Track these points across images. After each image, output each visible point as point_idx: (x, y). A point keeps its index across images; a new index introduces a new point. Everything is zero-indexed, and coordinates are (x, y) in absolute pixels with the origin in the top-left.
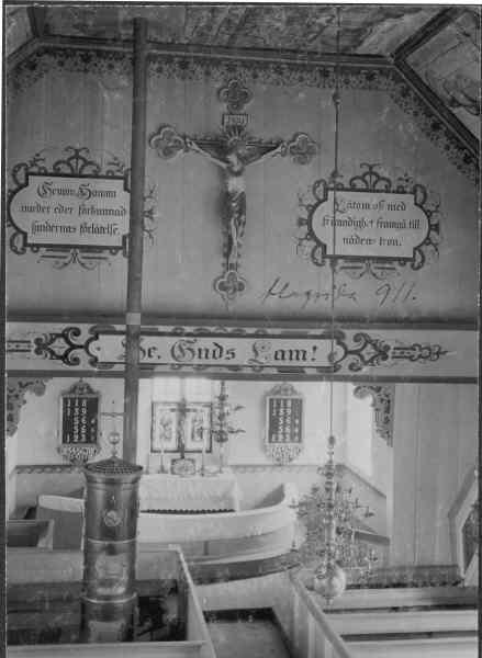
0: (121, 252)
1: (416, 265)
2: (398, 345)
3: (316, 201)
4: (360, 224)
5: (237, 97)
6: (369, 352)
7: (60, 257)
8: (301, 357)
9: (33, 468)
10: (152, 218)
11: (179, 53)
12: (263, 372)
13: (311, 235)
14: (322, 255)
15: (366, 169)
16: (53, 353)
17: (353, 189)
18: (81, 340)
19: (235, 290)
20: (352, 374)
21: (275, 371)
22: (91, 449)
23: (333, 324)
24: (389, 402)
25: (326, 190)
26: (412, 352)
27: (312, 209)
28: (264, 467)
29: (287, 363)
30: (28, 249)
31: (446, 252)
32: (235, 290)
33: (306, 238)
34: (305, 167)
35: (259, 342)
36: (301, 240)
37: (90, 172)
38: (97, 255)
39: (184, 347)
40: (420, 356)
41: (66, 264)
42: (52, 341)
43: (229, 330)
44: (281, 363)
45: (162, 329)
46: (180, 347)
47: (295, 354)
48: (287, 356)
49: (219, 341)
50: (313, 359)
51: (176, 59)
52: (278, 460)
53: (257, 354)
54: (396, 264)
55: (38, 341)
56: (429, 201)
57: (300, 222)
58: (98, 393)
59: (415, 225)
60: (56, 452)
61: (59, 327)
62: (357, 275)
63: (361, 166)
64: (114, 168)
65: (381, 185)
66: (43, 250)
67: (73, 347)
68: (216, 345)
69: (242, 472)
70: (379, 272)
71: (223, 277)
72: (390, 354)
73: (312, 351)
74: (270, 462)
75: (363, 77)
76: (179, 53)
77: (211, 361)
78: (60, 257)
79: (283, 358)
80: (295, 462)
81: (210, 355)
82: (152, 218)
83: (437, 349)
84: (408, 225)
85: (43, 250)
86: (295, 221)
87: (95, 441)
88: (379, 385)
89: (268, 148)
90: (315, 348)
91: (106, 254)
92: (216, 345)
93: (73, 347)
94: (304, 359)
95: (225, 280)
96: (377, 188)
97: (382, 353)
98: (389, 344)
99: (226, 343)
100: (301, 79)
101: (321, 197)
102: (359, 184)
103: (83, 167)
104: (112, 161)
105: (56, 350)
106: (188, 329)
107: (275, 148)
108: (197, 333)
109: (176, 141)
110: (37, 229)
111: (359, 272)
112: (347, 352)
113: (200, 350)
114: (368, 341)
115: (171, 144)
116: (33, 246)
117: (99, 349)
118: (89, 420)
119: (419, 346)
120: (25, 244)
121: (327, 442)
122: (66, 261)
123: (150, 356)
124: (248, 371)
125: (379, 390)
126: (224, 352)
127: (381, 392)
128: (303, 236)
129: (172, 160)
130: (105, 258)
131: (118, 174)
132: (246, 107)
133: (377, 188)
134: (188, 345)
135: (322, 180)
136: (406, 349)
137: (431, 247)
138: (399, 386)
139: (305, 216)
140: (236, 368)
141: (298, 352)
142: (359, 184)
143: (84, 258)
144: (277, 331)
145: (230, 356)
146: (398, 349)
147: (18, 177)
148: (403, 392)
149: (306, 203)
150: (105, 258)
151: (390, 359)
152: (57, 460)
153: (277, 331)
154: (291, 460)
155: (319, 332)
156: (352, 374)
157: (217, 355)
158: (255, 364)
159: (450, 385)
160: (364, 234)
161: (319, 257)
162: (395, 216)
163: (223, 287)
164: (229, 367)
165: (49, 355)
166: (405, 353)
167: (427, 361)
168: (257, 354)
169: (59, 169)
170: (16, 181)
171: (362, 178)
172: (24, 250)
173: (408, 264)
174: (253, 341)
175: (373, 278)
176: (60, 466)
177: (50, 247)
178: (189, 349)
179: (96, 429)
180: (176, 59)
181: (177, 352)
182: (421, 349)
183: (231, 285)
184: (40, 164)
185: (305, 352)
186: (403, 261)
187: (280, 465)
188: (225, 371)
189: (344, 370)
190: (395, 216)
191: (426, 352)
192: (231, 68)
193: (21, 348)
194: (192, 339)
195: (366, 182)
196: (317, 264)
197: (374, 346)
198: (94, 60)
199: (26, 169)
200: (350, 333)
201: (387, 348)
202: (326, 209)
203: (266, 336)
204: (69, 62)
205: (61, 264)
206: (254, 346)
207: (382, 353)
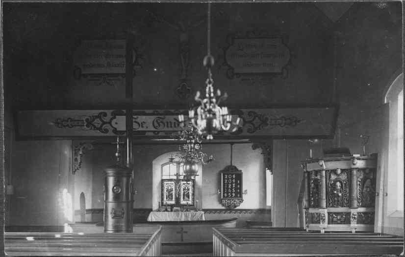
30: (235, 76)
42: (94, 120)
46: (157, 121)
55: (87, 120)
61: (96, 112)
83: (60, 126)
105: (96, 125)
114: (100, 129)
117: (116, 123)
138: (275, 141)
151: (269, 126)
165: (93, 128)
178: (162, 122)
181: (156, 124)
193: (80, 124)
194: (162, 117)
197: (260, 118)
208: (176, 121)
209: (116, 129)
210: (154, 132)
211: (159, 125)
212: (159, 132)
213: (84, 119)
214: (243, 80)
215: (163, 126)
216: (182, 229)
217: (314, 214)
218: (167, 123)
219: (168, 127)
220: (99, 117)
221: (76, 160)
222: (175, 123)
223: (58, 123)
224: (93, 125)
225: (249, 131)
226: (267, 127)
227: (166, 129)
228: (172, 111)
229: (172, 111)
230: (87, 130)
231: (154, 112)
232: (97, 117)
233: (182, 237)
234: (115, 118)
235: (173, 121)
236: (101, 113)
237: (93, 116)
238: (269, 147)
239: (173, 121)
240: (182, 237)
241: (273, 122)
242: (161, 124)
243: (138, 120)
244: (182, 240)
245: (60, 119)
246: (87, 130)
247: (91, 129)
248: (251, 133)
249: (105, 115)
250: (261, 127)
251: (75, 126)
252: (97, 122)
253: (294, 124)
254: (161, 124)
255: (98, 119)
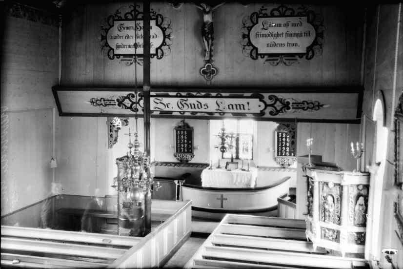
0: (156, 57)
1: (309, 57)
2: (294, 101)
4: (278, 35)
6: (278, 105)
7: (130, 60)
8: (242, 108)
9: (162, 164)
10: (169, 39)
12: (197, 115)
14: (255, 54)
16: (126, 106)
18: (269, 109)
19: (211, 74)
20: (272, 117)
22: (189, 156)
23: (256, 90)
24: (294, 132)
26: (303, 106)
28: (275, 168)
30: (115, 57)
31: (326, 49)
33: (247, 45)
35: (219, 100)
36: (245, 46)
37: (289, 14)
39: (183, 103)
40: (308, 108)
42: (124, 100)
45: (171, 94)
46: (181, 103)
47: (238, 106)
48: (235, 107)
49: (200, 100)
50: (249, 109)
52: (283, 165)
54: (297, 57)
55: (118, 100)
57: (244, 36)
58: (192, 128)
59: (308, 34)
60: (173, 156)
61: (125, 94)
65: (288, 13)
68: (198, 101)
69: (264, 170)
70: (287, 62)
71: (204, 67)
72: (290, 106)
73: (247, 105)
74: (279, 166)
77: (197, 110)
78: (130, 60)
79: (233, 108)
80: (291, 166)
83: (317, 104)
84: (303, 35)
85: (122, 57)
87: (192, 152)
88: (288, 123)
90: (248, 103)
92: (198, 101)
94: (244, 109)
95: (205, 68)
96: (286, 14)
97: (286, 106)
98: (289, 101)
99: (203, 101)
102: (130, 17)
103: (286, 11)
105: (126, 104)
106: (184, 94)
108: (188, 96)
110: (118, 47)
118: (188, 141)
119: (307, 102)
121: (118, 140)
123: (168, 107)
125: (288, 126)
126: (203, 106)
127: (290, 127)
131: (304, 14)
133: (286, 14)
134: (184, 102)
135: (256, 13)
136: (299, 103)
137: (166, 47)
138: (299, 124)
141: (240, 105)
143: (139, 60)
144: (227, 94)
145: (206, 107)
146: (295, 103)
148: (301, 128)
150: (296, 60)
151: (291, 109)
152: (174, 160)
154: (289, 165)
156: (272, 117)
157: (200, 107)
159: (309, 124)
160: (278, 41)
161: (254, 55)
162: (297, 30)
163: (204, 72)
165: (124, 107)
166: (299, 106)
167: (313, 110)
170: (109, 25)
171: (130, 13)
172: (257, 58)
173: (305, 57)
174: (215, 99)
175: (284, 65)
176: (173, 163)
177: (125, 56)
178: (185, 104)
179: (192, 146)
182: (308, 104)
183: (208, 71)
184: (119, 15)
185: (243, 105)
186: (301, 55)
187: (284, 168)
188: (206, 115)
189: (267, 115)
190: (297, 30)
191: (311, 105)
193: (112, 103)
194: (185, 99)
196: (253, 58)
197: (281, 102)
199: (113, 18)
200: (266, 96)
201: (288, 103)
202: (257, 28)
203: (222, 97)
205: (130, 64)
206: (217, 102)
207: (286, 106)
209: (260, 100)
210: (180, 112)
212: (184, 112)
213: (116, 100)
215: (218, 102)
216: (222, 196)
217: (289, 156)
218: (191, 104)
219: (191, 108)
220: (128, 97)
221: (111, 136)
222: (198, 105)
223: (93, 102)
224: (125, 105)
226: (289, 111)
227: (190, 110)
228: (195, 94)
229: (195, 94)
230: (289, 98)
231: (177, 94)
232: (126, 98)
233: (222, 204)
234: (261, 111)
235: (196, 103)
236: (129, 95)
238: (293, 129)
240: (222, 204)
241: (295, 106)
242: (185, 105)
243: (188, 103)
244: (222, 207)
245: (94, 99)
246: (289, 98)
247: (285, 99)
248: (131, 94)
249: (271, 113)
251: (108, 105)
252: (127, 102)
253: (317, 108)
255: (128, 100)
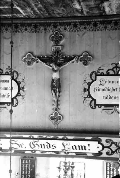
3: (91, 81)
5: (57, 39)
10: (23, 91)
11: (113, 19)
13: (89, 96)
15: (114, 65)
17: (108, 75)
21: (74, 154)
25: (96, 75)
27: (89, 84)
29: (78, 151)
30: (97, 106)
32: (57, 119)
33: (87, 97)
34: (86, 67)
35: (65, 142)
38: (2, 106)
41: (112, 113)
43: (52, 137)
44: (75, 151)
48: (78, 148)
49: (49, 141)
51: (53, 24)
53: (65, 147)
56: (19, 77)
57: (85, 90)
62: (110, 113)
63: (112, 64)
64: (8, 71)
66: (103, 107)
67: (108, 147)
75: (92, 25)
76: (113, 19)
77: (46, 149)
81: (46, 147)
82: (23, 91)
86: (82, 90)
89: (70, 59)
90: (89, 145)
91: (6, 105)
93: (108, 147)
99: (52, 142)
100: (85, 28)
101: (94, 79)
104: (8, 68)
107: (73, 59)
108: (39, 138)
109: (33, 58)
111: (111, 111)
112: (104, 147)
113: (41, 145)
114: (113, 143)
115: (30, 60)
116: (98, 105)
117: (98, 148)
120: (95, 104)
122: (113, 111)
124: (63, 154)
128: (86, 96)
129: (31, 67)
130: (5, 107)
132: (62, 42)
137: (21, 97)
139: (87, 87)
140: (58, 152)
141: (82, 146)
142: (111, 72)
144: (72, 138)
147: (92, 77)
149: (87, 82)
150: (5, 107)
153: (72, 138)
155: (90, 138)
158: (65, 151)
161: (93, 105)
163: (52, 118)
164: (55, 152)
168: (65, 147)
169: (109, 73)
171: (112, 70)
172: (95, 108)
178: (36, 144)
180: (53, 24)
181: (32, 146)
184: (101, 71)
192: (55, 27)
194: (37, 140)
195: (114, 71)
196: (92, 108)
197: (116, 145)
198: (20, 27)
200: (104, 139)
204: (109, 26)
208: (47, 144)
210: (32, 151)
211: (35, 146)
212: (35, 151)
214: (103, 110)
215: (38, 147)
220: (113, 152)
222: (47, 145)
225: (107, 153)
227: (40, 149)
234: (99, 152)
236: (111, 155)
237: (117, 153)
239: (46, 144)
242: (36, 145)
250: (118, 151)
252: (114, 147)
254: (36, 145)
